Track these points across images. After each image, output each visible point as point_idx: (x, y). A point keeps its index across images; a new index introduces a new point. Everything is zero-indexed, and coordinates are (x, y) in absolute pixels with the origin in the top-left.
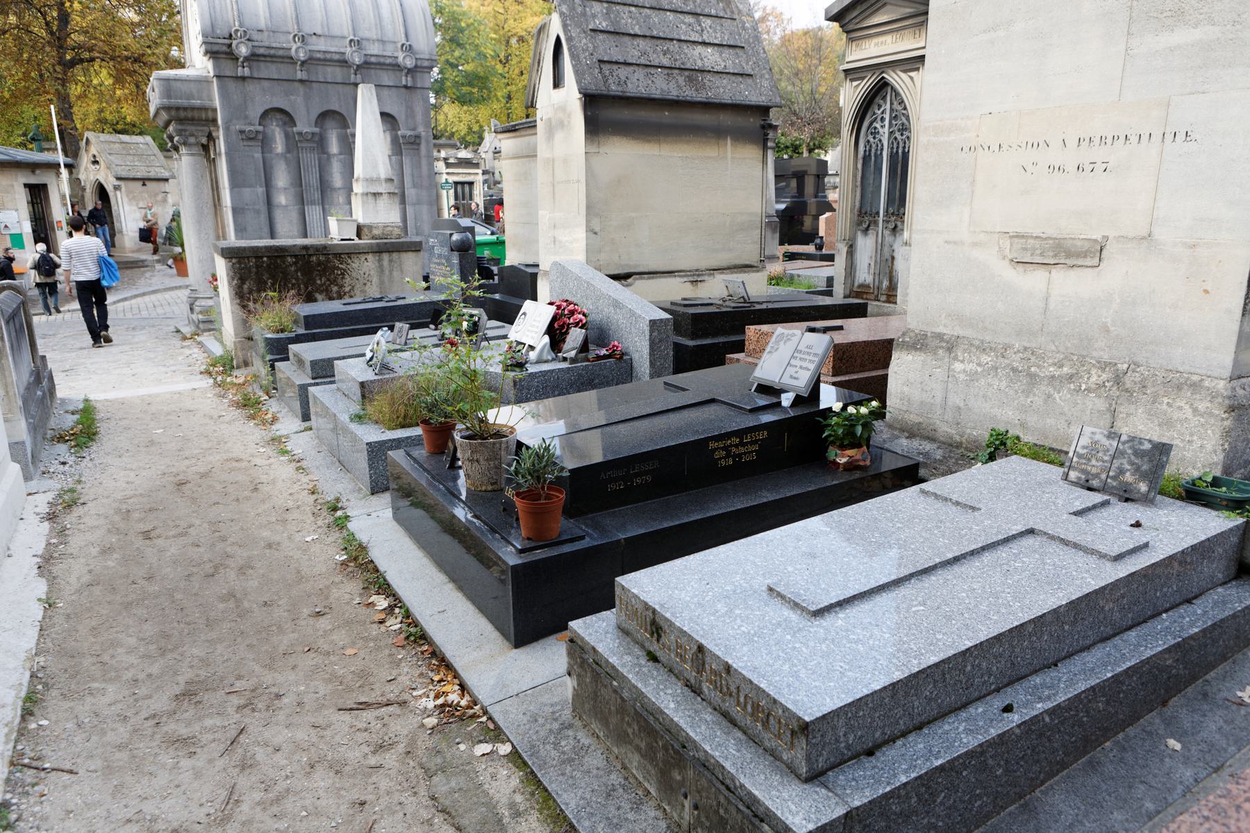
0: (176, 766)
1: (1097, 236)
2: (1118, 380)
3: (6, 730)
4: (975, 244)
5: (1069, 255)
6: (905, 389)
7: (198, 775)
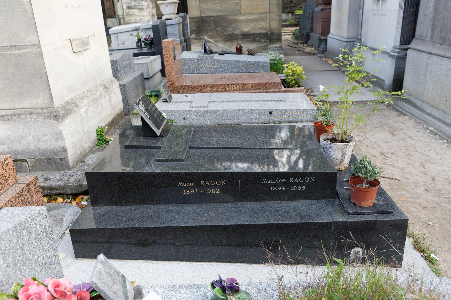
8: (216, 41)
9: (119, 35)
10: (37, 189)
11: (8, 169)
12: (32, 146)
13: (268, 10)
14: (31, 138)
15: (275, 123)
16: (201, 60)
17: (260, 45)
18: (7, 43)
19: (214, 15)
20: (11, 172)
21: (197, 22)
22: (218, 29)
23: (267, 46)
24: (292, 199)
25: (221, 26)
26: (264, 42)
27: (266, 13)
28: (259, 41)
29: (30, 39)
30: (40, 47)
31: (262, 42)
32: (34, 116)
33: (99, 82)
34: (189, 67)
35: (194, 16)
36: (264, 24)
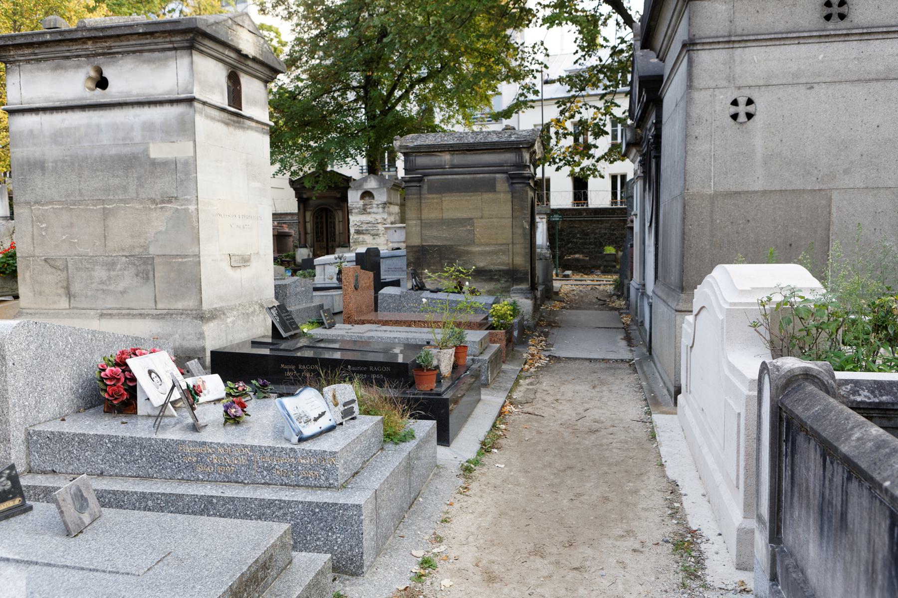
9: (327, 267)
18: (174, 253)
23: (509, 287)
25: (448, 259)
32: (183, 316)
33: (255, 299)
34: (388, 305)
36: (505, 258)
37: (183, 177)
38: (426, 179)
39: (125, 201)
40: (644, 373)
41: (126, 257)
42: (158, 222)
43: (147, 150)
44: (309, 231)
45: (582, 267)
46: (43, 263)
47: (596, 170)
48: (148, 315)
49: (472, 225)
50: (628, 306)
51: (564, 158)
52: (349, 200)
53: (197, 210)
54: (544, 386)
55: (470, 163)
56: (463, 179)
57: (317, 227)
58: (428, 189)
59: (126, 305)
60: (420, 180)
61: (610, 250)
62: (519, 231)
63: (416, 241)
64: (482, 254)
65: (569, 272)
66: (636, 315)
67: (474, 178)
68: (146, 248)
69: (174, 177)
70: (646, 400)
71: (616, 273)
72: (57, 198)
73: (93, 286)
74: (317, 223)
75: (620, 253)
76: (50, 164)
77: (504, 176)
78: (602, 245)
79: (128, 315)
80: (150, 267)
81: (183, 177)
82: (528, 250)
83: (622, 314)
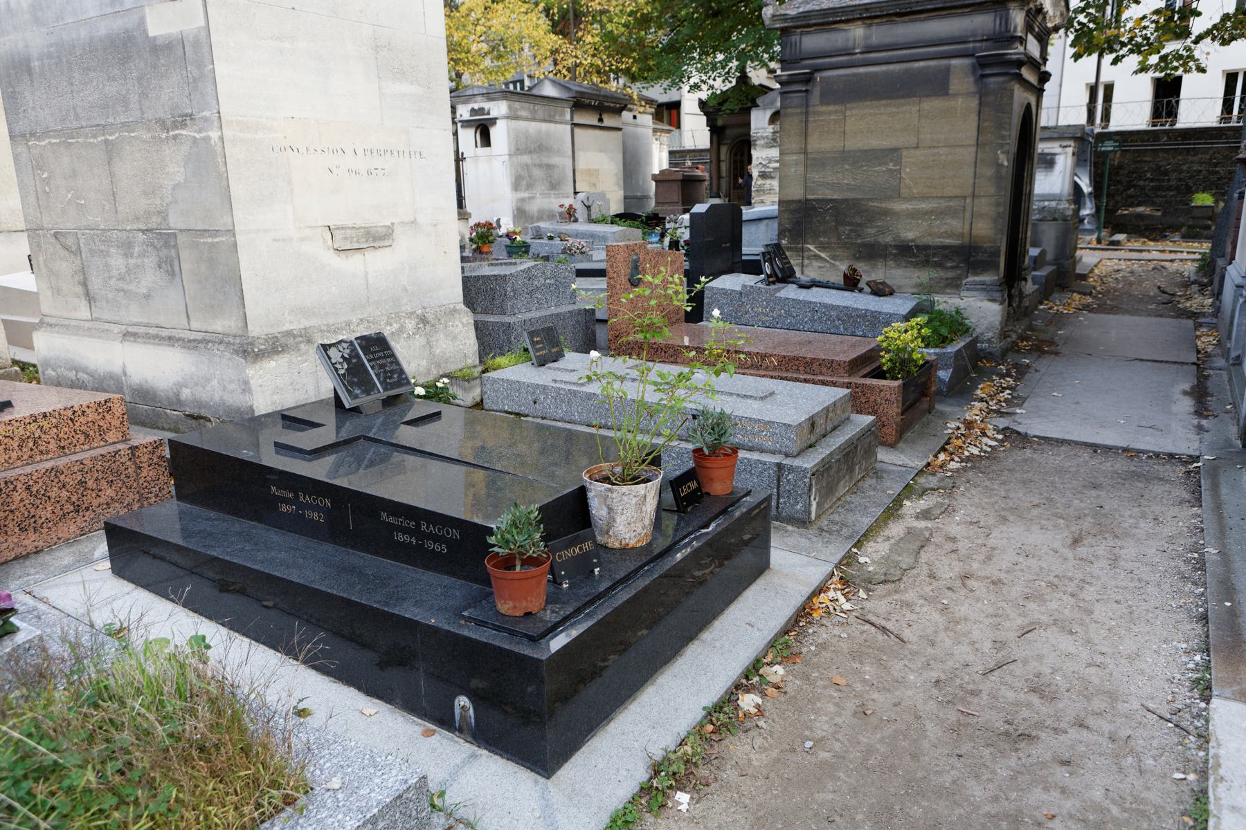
0: (1054, 671)
1: (388, 224)
2: (423, 320)
3: (1222, 772)
4: (302, 239)
5: (376, 238)
6: (275, 397)
7: (1040, 658)
8: (834, 258)
10: (155, 460)
11: (108, 417)
12: (217, 398)
13: (971, 190)
14: (215, 383)
15: (543, 418)
16: (747, 295)
17: (942, 274)
19: (836, 197)
20: (116, 423)
21: (795, 211)
22: (841, 229)
23: (959, 278)
24: (427, 568)
25: (850, 224)
26: (952, 268)
27: (965, 198)
28: (939, 265)
29: (222, 223)
30: (234, 235)
31: (947, 268)
32: (222, 347)
35: (790, 198)
36: (955, 225)
37: (196, 73)
38: (818, 76)
39: (126, 126)
40: (1218, 507)
41: (143, 231)
42: (174, 167)
43: (142, 22)
44: (724, 173)
45: (1147, 228)
46: (53, 240)
47: (1191, 57)
48: (179, 340)
49: (898, 161)
50: (1217, 311)
51: (1131, 39)
52: (753, 126)
53: (221, 138)
54: (954, 526)
55: (901, 40)
56: (886, 73)
57: (735, 169)
58: (822, 95)
59: (153, 321)
60: (808, 79)
61: (1204, 199)
62: (989, 172)
63: (796, 193)
64: (914, 215)
65: (1120, 237)
66: (1229, 337)
67: (907, 71)
68: (163, 214)
69: (184, 73)
70: (1204, 618)
71: (1207, 238)
72: (53, 126)
73: (112, 282)
74: (735, 162)
75: (1222, 204)
76: (37, 63)
77: (967, 61)
78: (1190, 191)
79: (156, 337)
80: (173, 253)
81: (196, 73)
82: (1005, 209)
83: (1201, 325)
